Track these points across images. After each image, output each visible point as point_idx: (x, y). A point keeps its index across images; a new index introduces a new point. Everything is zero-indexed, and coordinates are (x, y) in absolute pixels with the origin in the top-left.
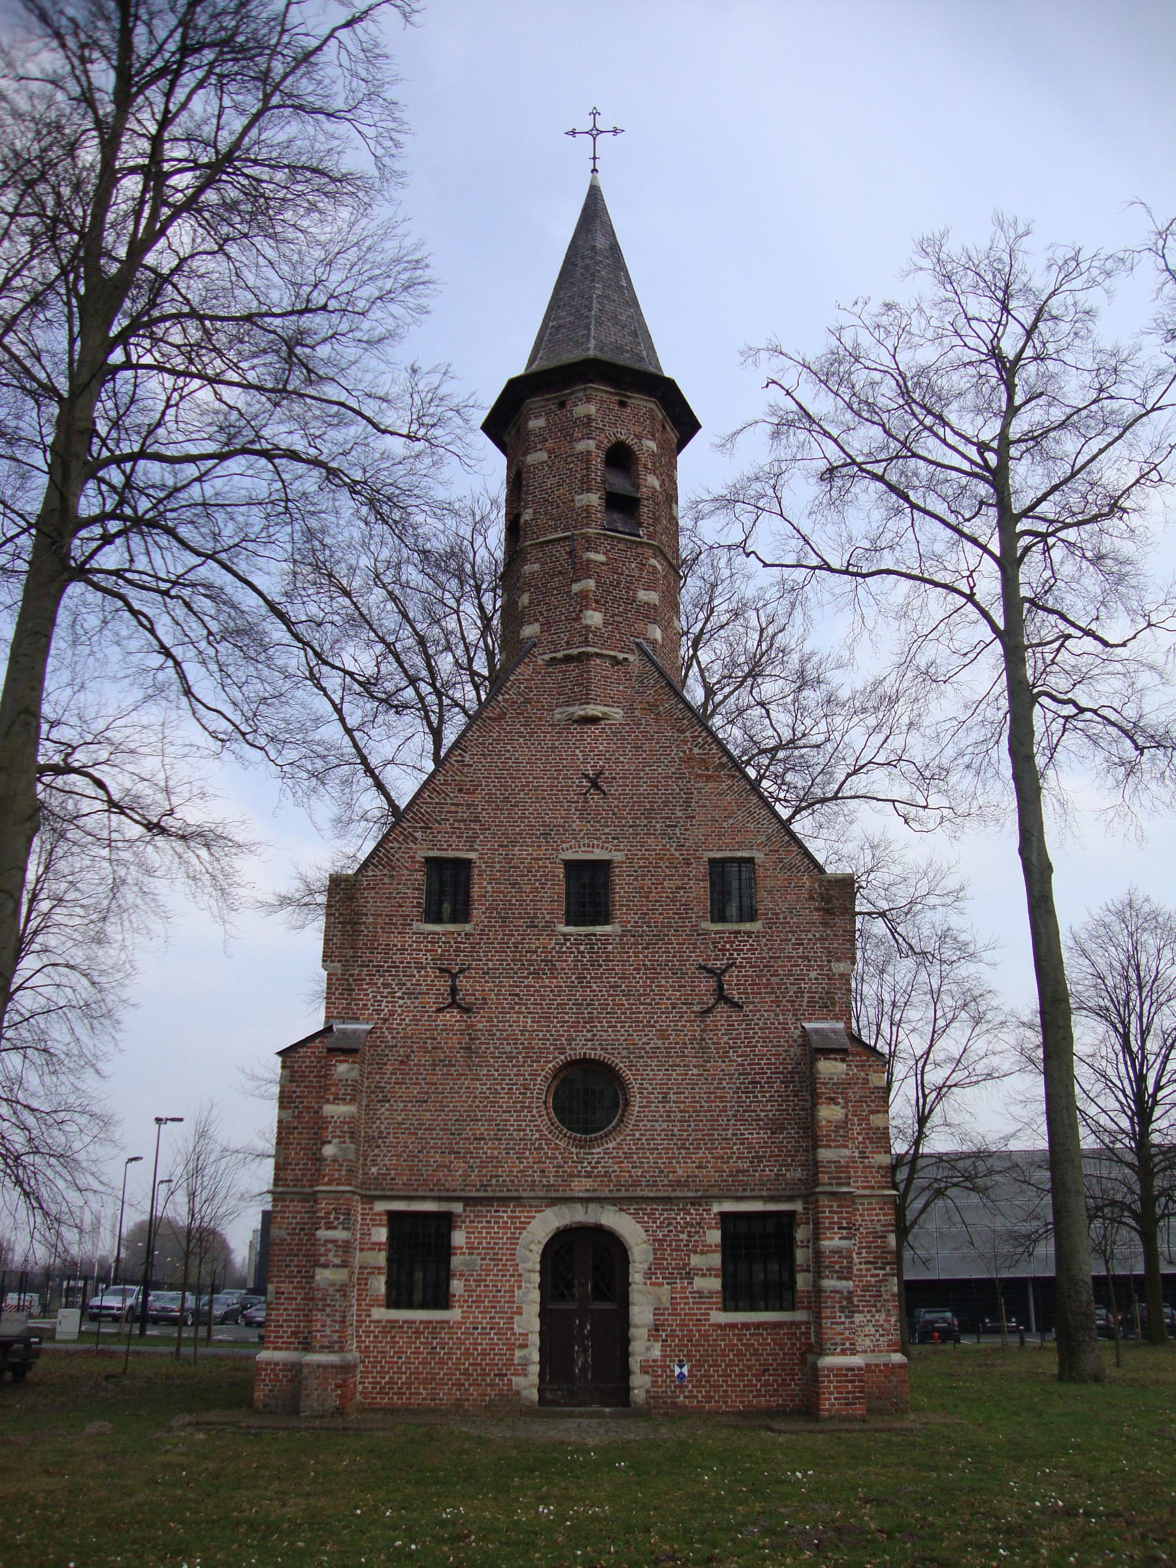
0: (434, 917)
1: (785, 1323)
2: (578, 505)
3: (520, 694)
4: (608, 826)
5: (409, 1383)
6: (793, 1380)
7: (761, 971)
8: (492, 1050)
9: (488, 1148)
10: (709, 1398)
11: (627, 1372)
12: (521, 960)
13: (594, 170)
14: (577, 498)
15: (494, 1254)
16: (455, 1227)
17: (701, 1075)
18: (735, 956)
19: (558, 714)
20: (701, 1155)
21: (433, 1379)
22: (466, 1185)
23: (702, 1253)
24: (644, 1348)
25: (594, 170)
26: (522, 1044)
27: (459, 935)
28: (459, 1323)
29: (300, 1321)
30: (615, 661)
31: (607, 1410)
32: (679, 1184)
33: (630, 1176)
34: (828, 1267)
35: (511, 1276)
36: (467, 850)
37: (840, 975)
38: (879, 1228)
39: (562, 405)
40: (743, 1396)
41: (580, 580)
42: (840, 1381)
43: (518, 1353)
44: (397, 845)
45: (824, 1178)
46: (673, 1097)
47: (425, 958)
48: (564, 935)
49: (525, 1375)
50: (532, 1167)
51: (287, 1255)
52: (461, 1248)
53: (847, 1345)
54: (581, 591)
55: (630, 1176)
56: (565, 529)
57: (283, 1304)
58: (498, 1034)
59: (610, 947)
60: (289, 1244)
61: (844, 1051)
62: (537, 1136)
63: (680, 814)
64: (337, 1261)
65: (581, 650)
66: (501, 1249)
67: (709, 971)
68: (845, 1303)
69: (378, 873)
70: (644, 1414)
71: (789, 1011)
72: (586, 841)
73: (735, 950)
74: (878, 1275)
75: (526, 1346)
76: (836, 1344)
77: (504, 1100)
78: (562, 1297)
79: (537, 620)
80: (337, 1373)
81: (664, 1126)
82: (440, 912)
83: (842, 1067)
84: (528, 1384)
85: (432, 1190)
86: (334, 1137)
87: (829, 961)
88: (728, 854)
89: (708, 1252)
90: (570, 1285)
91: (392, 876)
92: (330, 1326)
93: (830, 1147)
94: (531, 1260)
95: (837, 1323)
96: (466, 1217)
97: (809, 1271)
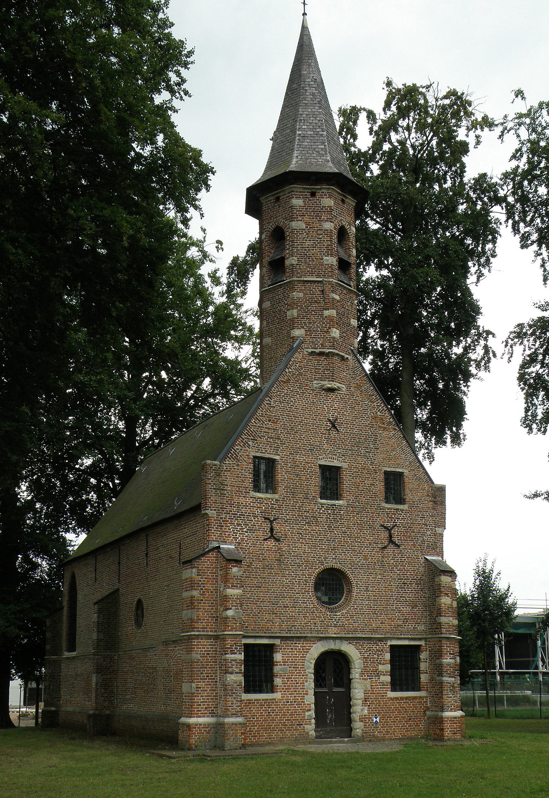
0: (257, 488)
1: (417, 697)
3: (296, 370)
4: (340, 449)
7: (407, 529)
8: (290, 561)
10: (388, 732)
13: (304, 14)
14: (325, 258)
16: (276, 652)
17: (382, 579)
18: (396, 521)
19: (316, 384)
20: (382, 617)
21: (270, 728)
24: (359, 709)
25: (304, 14)
26: (304, 559)
27: (272, 500)
30: (343, 358)
32: (374, 631)
33: (353, 627)
34: (445, 672)
35: (303, 675)
36: (275, 455)
39: (313, 194)
41: (328, 309)
43: (307, 714)
44: (241, 448)
45: (444, 630)
47: (257, 512)
48: (321, 504)
49: (310, 724)
51: (202, 668)
52: (280, 662)
54: (329, 316)
55: (353, 627)
56: (318, 276)
57: (200, 693)
58: (293, 553)
60: (202, 662)
64: (237, 670)
66: (298, 662)
67: (385, 527)
69: (231, 462)
71: (419, 550)
72: (330, 456)
73: (396, 518)
75: (310, 710)
76: (448, 707)
81: (367, 603)
84: (311, 728)
85: (265, 633)
86: (232, 606)
87: (435, 527)
89: (386, 663)
90: (324, 679)
91: (238, 465)
92: (236, 704)
93: (446, 616)
94: (310, 669)
95: (449, 697)
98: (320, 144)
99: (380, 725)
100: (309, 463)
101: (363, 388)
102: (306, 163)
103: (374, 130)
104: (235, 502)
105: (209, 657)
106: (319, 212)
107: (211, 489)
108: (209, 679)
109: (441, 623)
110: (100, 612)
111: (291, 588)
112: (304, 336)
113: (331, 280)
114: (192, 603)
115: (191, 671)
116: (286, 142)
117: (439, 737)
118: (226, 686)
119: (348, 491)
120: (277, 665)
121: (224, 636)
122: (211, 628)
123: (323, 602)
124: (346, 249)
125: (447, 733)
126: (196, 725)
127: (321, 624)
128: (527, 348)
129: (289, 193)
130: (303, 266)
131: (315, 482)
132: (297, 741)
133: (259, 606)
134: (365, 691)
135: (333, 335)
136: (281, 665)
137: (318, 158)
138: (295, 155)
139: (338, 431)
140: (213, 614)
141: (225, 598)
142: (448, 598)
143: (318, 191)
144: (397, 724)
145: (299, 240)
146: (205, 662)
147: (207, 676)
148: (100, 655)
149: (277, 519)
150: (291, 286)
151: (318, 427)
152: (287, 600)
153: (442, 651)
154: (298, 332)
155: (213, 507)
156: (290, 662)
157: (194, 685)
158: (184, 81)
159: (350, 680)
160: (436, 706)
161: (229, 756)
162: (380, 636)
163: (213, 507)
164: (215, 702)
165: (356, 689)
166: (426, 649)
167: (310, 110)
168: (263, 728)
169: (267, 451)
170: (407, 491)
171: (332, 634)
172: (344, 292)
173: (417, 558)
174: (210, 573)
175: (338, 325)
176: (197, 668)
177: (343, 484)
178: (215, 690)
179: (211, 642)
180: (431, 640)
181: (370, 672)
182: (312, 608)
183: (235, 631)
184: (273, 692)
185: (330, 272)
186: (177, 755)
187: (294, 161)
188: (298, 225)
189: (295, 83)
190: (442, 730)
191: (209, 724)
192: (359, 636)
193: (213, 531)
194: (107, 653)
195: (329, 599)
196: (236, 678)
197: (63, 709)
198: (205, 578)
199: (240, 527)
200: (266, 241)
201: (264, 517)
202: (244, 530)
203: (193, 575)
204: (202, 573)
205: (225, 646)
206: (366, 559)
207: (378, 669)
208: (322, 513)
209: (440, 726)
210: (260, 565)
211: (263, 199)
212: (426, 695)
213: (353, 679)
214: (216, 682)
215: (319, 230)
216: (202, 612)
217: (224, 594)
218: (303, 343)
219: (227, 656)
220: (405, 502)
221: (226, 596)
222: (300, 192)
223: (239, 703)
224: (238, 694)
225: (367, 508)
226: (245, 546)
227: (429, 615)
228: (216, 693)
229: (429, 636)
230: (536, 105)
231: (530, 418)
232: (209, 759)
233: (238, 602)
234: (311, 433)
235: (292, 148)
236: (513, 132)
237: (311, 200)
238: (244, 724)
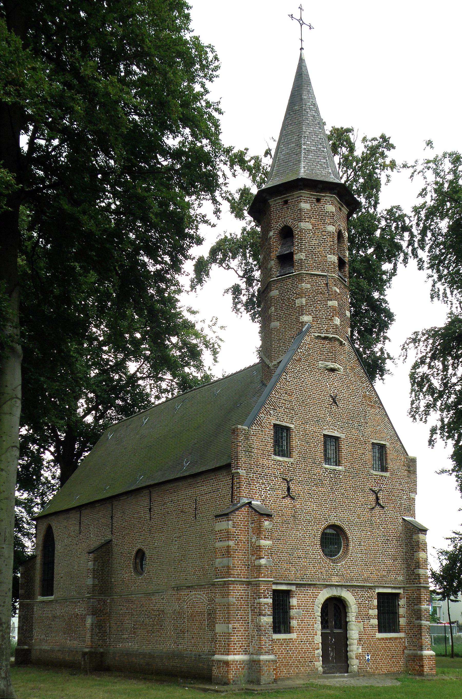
2: (329, 260)
4: (339, 422)
6: (400, 661)
9: (303, 562)
12: (311, 478)
13: (302, 49)
14: (328, 256)
15: (307, 609)
16: (293, 597)
17: (371, 535)
19: (321, 364)
21: (288, 665)
22: (296, 578)
24: (355, 649)
26: (313, 516)
27: (289, 463)
28: (296, 639)
29: (243, 641)
30: (341, 344)
32: (365, 580)
33: (350, 576)
35: (313, 618)
36: (290, 423)
39: (318, 200)
41: (332, 300)
44: (264, 416)
47: (277, 473)
48: (325, 469)
49: (319, 661)
51: (237, 610)
52: (295, 606)
55: (350, 576)
56: (323, 271)
57: (236, 633)
59: (341, 476)
60: (237, 605)
63: (363, 421)
64: (269, 613)
67: (373, 491)
69: (257, 428)
72: (332, 427)
73: (381, 484)
75: (318, 649)
84: (319, 664)
85: (284, 580)
87: (409, 492)
89: (375, 608)
93: (423, 569)
97: (405, 617)
98: (322, 158)
99: (371, 662)
100: (316, 432)
102: (312, 173)
105: (243, 601)
106: (324, 216)
107: (241, 450)
108: (243, 620)
109: (419, 574)
110: (95, 560)
111: (303, 541)
112: (311, 322)
113: (334, 275)
114: (228, 552)
115: (228, 613)
116: (292, 154)
117: (421, 673)
118: (260, 626)
120: (293, 609)
121: (258, 582)
125: (426, 669)
126: (234, 661)
127: (326, 573)
128: (419, 352)
129: (297, 197)
133: (279, 556)
134: (360, 632)
138: (303, 165)
139: (338, 406)
143: (322, 198)
144: (384, 661)
146: (239, 605)
147: (241, 618)
148: (95, 599)
150: (300, 278)
151: (323, 401)
152: (301, 551)
153: (421, 599)
154: (306, 318)
156: (303, 606)
157: (230, 626)
158: (207, 92)
159: (346, 623)
160: (414, 646)
165: (352, 630)
166: (404, 596)
167: (312, 129)
169: (284, 420)
170: (389, 461)
171: (334, 582)
174: (243, 526)
178: (247, 631)
179: (244, 587)
180: (409, 589)
181: (363, 616)
183: (267, 578)
184: (290, 632)
186: (218, 689)
187: (302, 170)
188: (306, 225)
192: (355, 584)
194: (102, 597)
196: (267, 620)
197: (37, 647)
198: (239, 530)
200: (274, 238)
201: (282, 478)
203: (230, 527)
204: (237, 525)
205: (259, 591)
206: (359, 518)
207: (369, 614)
208: (326, 477)
209: (419, 663)
211: (271, 202)
213: (350, 621)
214: (248, 623)
215: (323, 231)
216: (237, 560)
217: (257, 545)
219: (261, 600)
220: (388, 470)
221: (260, 546)
222: (307, 197)
223: (271, 642)
225: (359, 474)
227: (406, 567)
228: (249, 633)
229: (408, 586)
230: (440, 155)
231: (415, 410)
232: (256, 692)
233: (269, 552)
235: (299, 159)
236: (421, 174)
237: (316, 205)
238: (276, 661)
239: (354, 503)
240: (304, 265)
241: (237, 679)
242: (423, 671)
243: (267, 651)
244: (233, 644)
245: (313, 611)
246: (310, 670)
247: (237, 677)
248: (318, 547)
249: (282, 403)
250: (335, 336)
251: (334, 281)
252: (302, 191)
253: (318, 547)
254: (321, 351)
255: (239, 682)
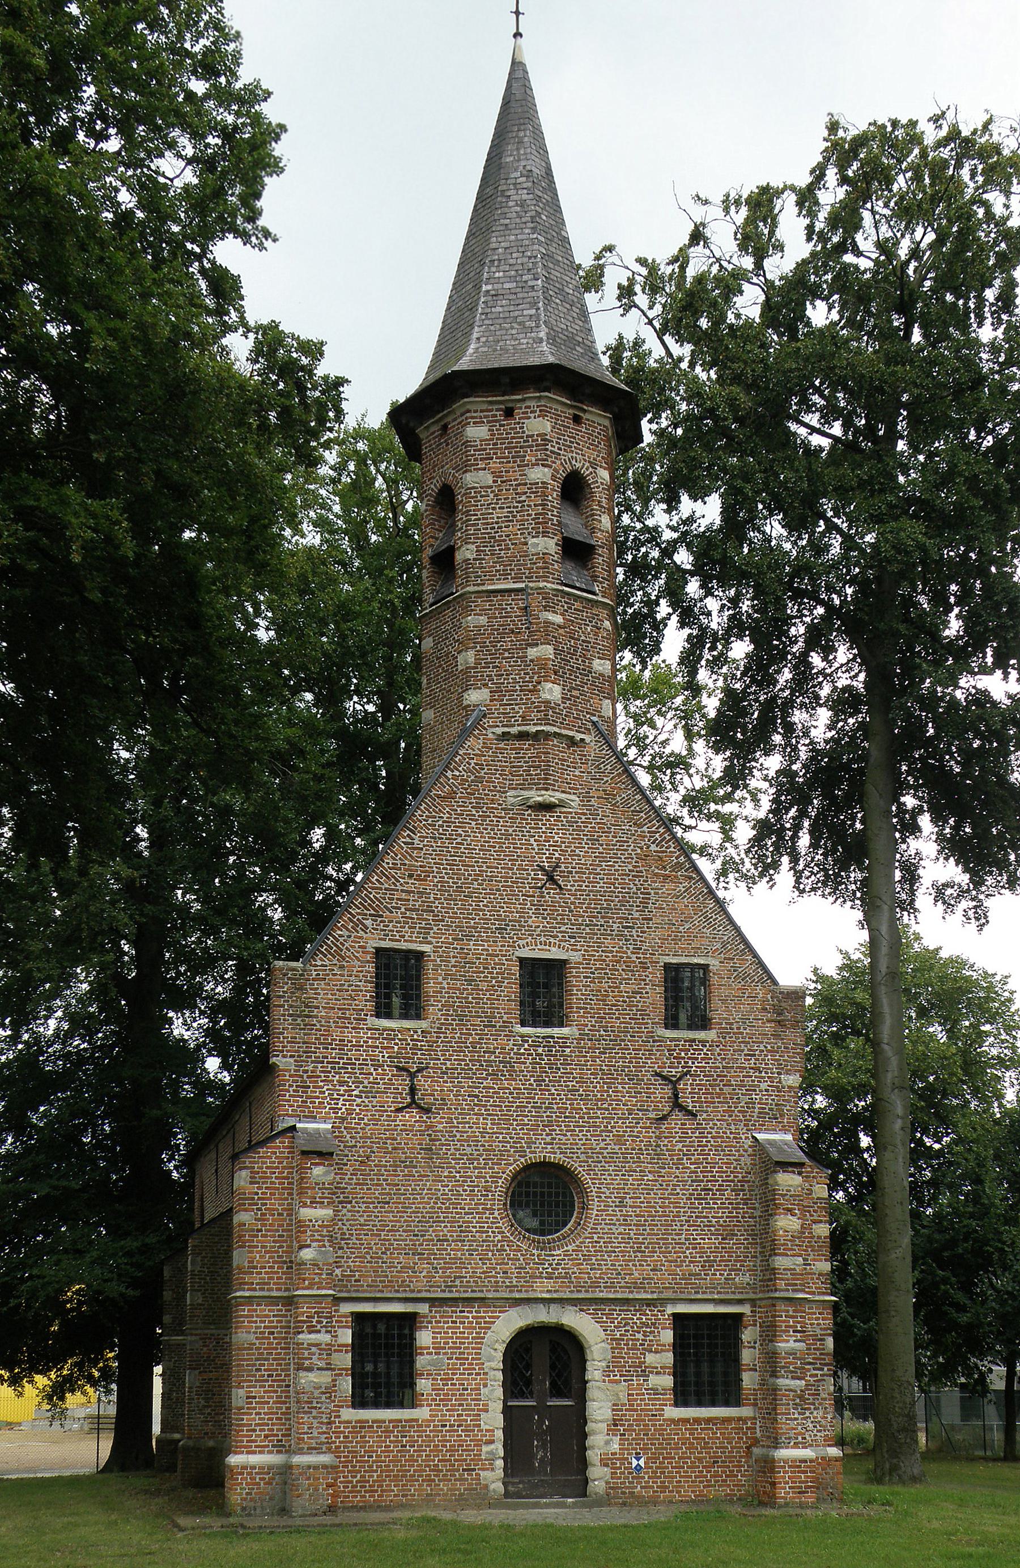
0: (383, 1011)
5: (380, 1481)
8: (452, 1151)
9: (452, 1251)
10: (663, 1488)
11: (583, 1464)
12: (479, 1061)
13: (517, 35)
14: (532, 541)
19: (512, 797)
20: (656, 1258)
22: (430, 1286)
23: (656, 1352)
24: (600, 1441)
29: (272, 1425)
30: (572, 742)
31: (570, 1500)
32: (636, 1286)
34: (784, 1367)
35: (477, 1374)
36: (421, 942)
37: (789, 1087)
38: (819, 1332)
39: (509, 413)
40: (695, 1486)
42: (795, 1472)
44: (347, 933)
45: (781, 1284)
46: (630, 1202)
49: (493, 1470)
50: (495, 1269)
51: (257, 1360)
53: (800, 1438)
54: (539, 659)
56: (517, 579)
57: (255, 1408)
58: (458, 1135)
61: (802, 1165)
62: (499, 1237)
63: (636, 915)
64: (321, 1364)
65: (539, 728)
66: (468, 1348)
68: (798, 1401)
69: (327, 963)
70: (604, 1501)
72: (543, 939)
74: (817, 1375)
75: (492, 1442)
76: (789, 1438)
77: (466, 1202)
78: (522, 1395)
79: (485, 685)
80: (328, 1473)
81: (621, 1229)
82: (389, 1005)
83: (797, 1180)
84: (494, 1478)
85: (398, 1291)
87: (779, 1073)
88: (684, 960)
89: (662, 1351)
90: (528, 1383)
91: (342, 967)
93: (787, 1255)
95: (790, 1419)
96: (432, 1317)
100: (497, 955)
101: (618, 799)
103: (817, 229)
104: (335, 1040)
105: (274, 1338)
107: (284, 1015)
109: (775, 1269)
111: (453, 1204)
113: (541, 585)
119: (581, 1008)
120: (422, 1354)
122: (278, 1284)
123: (528, 1230)
124: (587, 517)
125: (784, 1492)
126: (244, 1468)
129: (462, 415)
130: (488, 561)
131: (508, 993)
132: (462, 1502)
133: (384, 1240)
134: (614, 1405)
135: (545, 696)
136: (431, 1354)
137: (521, 336)
140: (282, 1257)
141: (301, 1226)
142: (794, 1219)
145: (478, 510)
146: (265, 1349)
147: (269, 1376)
148: (196, 1335)
149: (423, 1069)
152: (445, 1227)
153: (776, 1326)
154: (475, 696)
155: (288, 1051)
161: (284, 1527)
162: (649, 1297)
163: (288, 1051)
164: (285, 1424)
165: (594, 1401)
168: (390, 1476)
170: (716, 1003)
171: (541, 1292)
172: (577, 605)
173: (735, 1138)
174: (276, 1178)
175: (558, 675)
176: (248, 1360)
177: (572, 995)
178: (285, 1403)
179: (278, 1310)
180: (764, 1303)
181: (627, 1367)
182: (499, 1241)
183: (318, 1288)
184: (413, 1406)
185: (541, 568)
188: (478, 478)
189: (491, 183)
190: (773, 1484)
191: (271, 1467)
192: (601, 1295)
193: (287, 1097)
195: (542, 1223)
198: (266, 1188)
199: (345, 1088)
201: (396, 1067)
202: (354, 1093)
207: (644, 1362)
208: (523, 1054)
210: (386, 1160)
211: (421, 432)
212: (752, 1415)
214: (288, 1386)
215: (520, 484)
218: (485, 716)
219: (300, 1336)
223: (324, 1427)
224: (323, 1410)
225: (624, 1041)
226: (356, 1123)
228: (288, 1408)
233: (325, 1233)
234: (501, 895)
237: (504, 425)
239: (607, 1109)
240: (473, 573)
241: (252, 1504)
242: (773, 1496)
243: (314, 1445)
244: (247, 1431)
245: (480, 1359)
246: (465, 1490)
247: (251, 1500)
248: (496, 1214)
249: (398, 899)
250: (542, 728)
251: (543, 598)
252: (466, 400)
253: (496, 1214)
254: (514, 767)
255: (258, 1512)
